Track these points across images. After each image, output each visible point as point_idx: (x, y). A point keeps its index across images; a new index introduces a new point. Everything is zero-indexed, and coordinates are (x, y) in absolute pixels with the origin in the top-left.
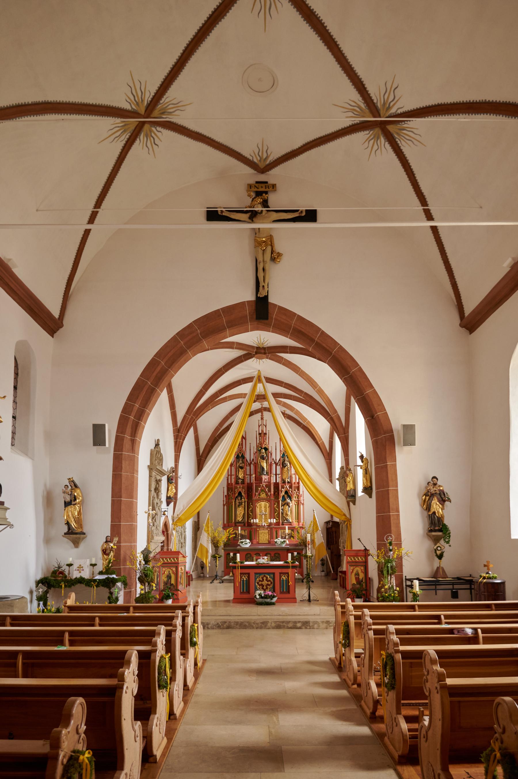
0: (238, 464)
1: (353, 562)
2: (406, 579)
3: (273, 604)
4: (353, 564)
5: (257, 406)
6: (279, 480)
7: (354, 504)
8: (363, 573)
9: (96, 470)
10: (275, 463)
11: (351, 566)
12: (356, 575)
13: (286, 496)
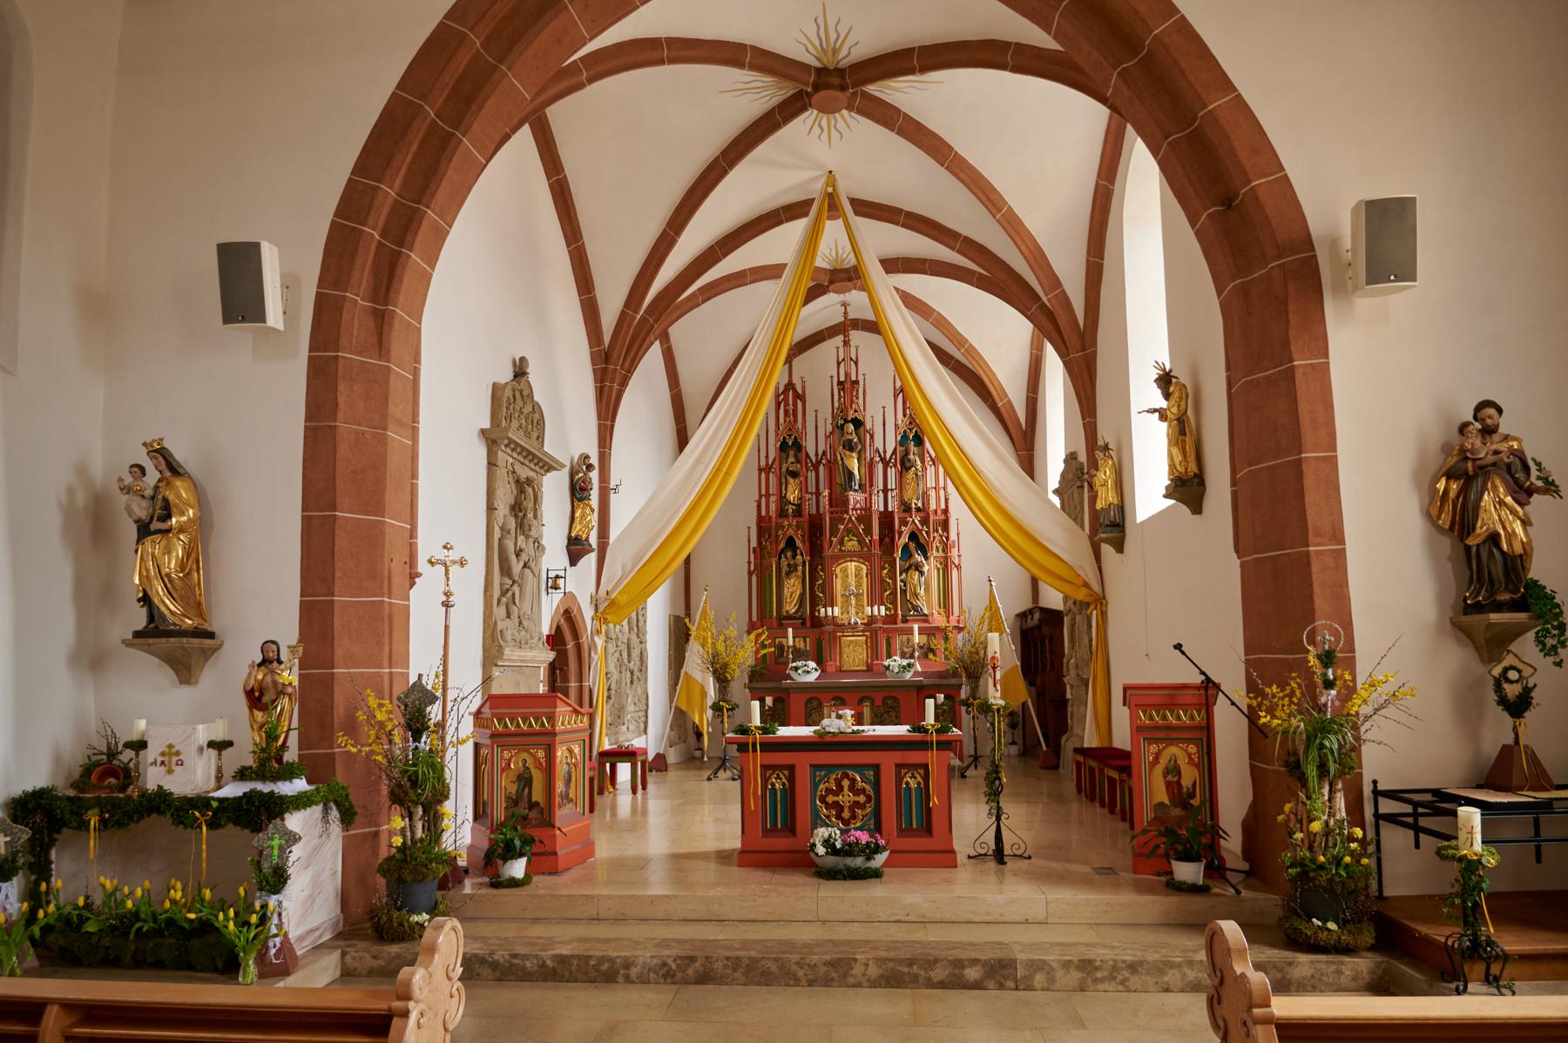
0: (784, 467)
1: (1157, 728)
2: (1377, 793)
3: (876, 874)
4: (1160, 734)
5: (826, 310)
6: (893, 505)
7: (1119, 547)
8: (1197, 766)
9: (247, 419)
10: (883, 460)
11: (1149, 740)
12: (1167, 772)
13: (912, 545)
